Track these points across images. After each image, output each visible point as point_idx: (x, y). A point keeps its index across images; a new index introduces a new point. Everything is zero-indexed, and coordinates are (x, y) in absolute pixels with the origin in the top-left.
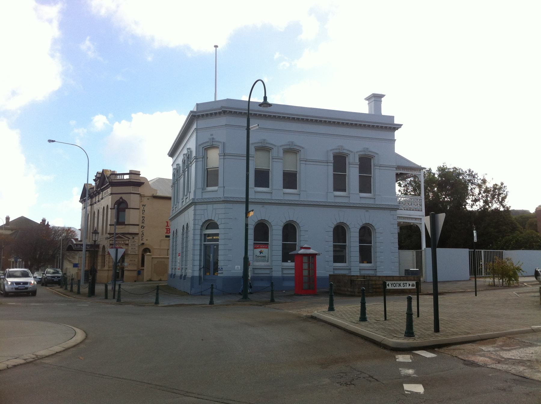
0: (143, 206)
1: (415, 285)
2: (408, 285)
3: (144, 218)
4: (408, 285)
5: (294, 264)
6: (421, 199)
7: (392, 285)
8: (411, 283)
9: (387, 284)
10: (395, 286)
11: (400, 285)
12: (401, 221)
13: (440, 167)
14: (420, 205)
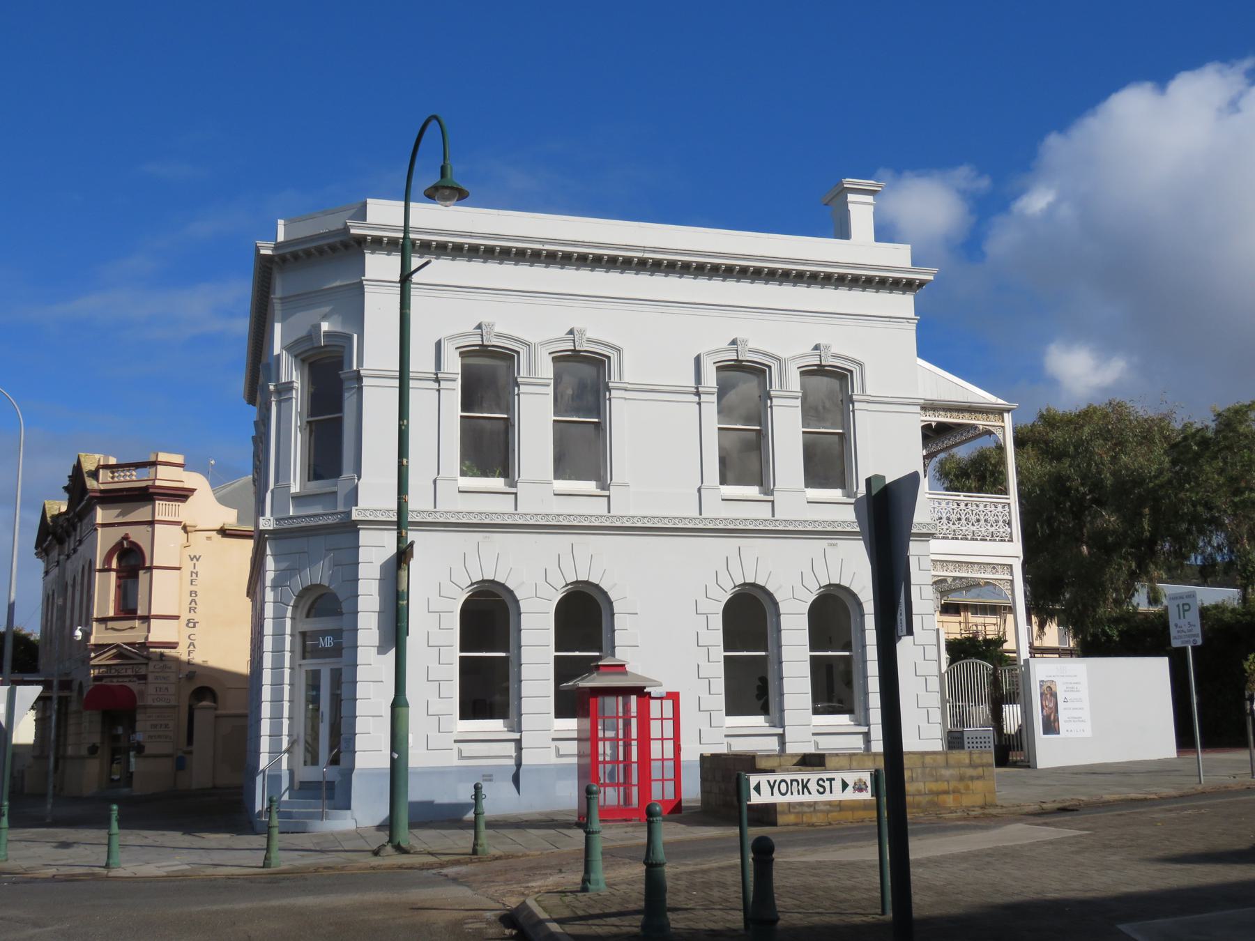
0: (192, 560)
1: (869, 784)
2: (837, 785)
3: (196, 595)
4: (837, 785)
6: (1009, 504)
7: (772, 788)
8: (851, 778)
9: (753, 785)
10: (783, 790)
11: (805, 786)
12: (945, 574)
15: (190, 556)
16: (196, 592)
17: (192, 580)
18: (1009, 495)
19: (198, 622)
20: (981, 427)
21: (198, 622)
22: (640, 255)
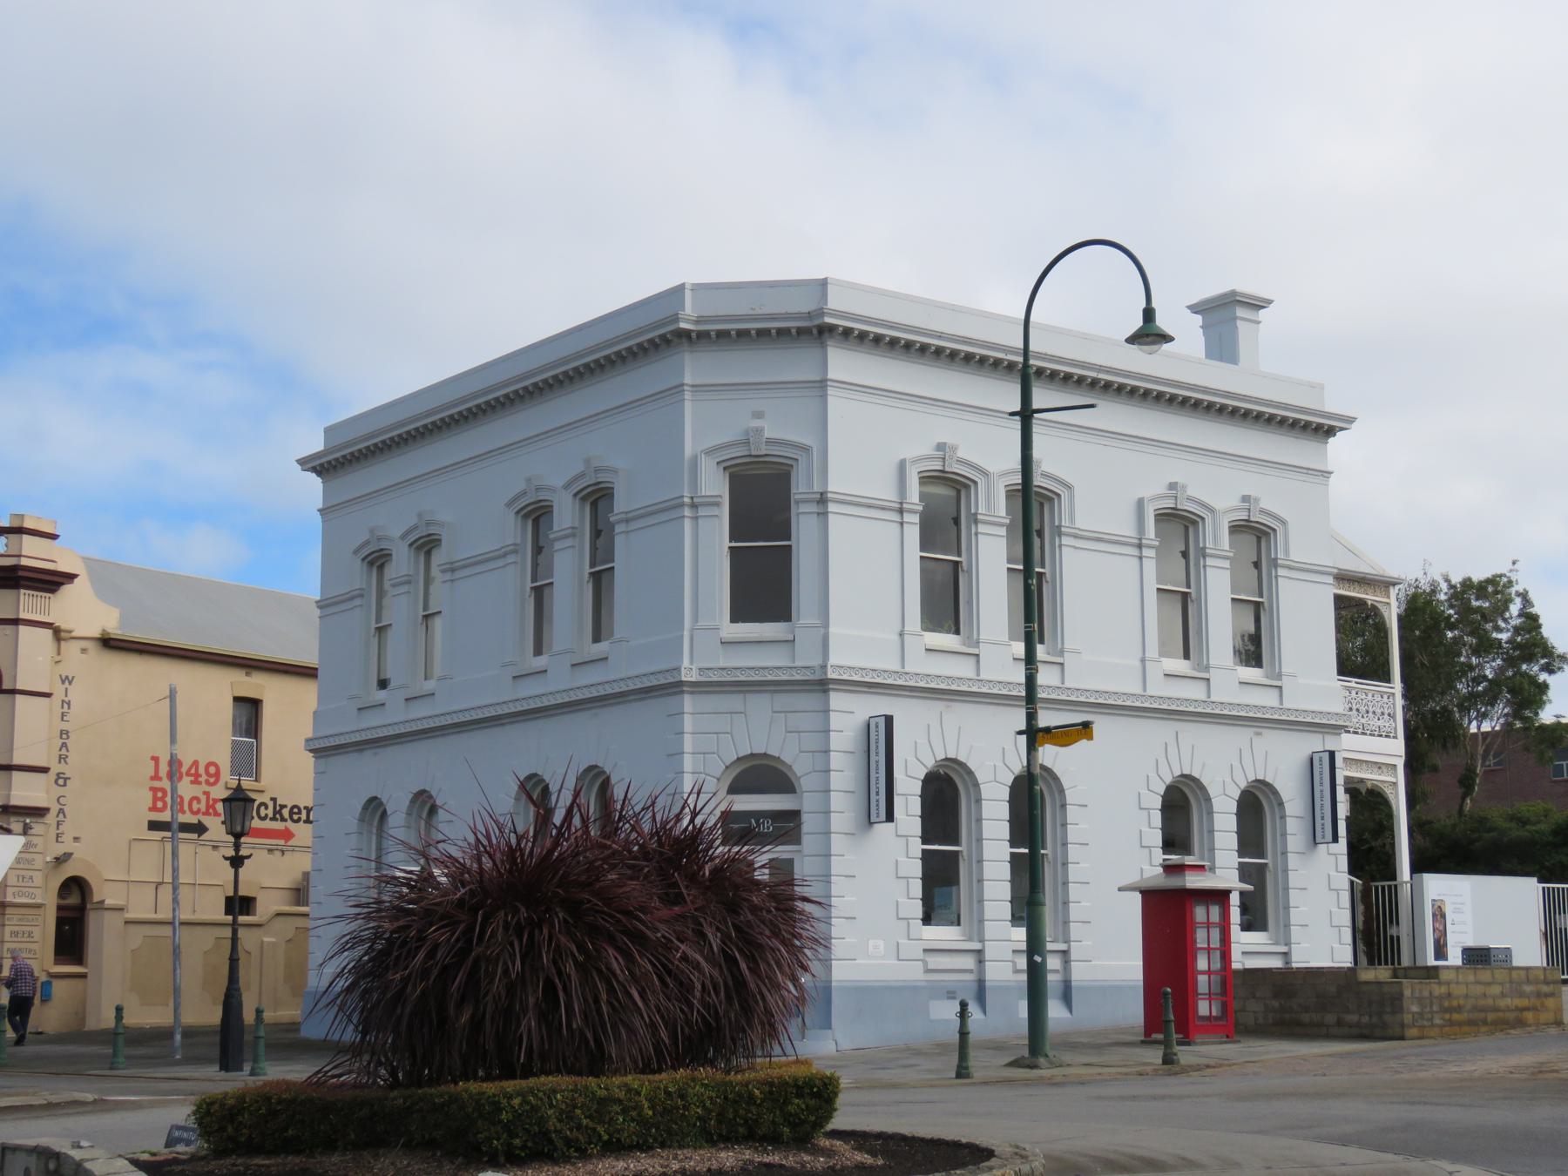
0: (63, 682)
3: (68, 738)
5: (1024, 937)
6: (1394, 694)
13: (1469, 579)
14: (1389, 715)
15: (61, 676)
16: (68, 732)
17: (63, 713)
18: (1394, 683)
19: (69, 778)
20: (1369, 602)
21: (69, 778)
22: (1093, 374)
